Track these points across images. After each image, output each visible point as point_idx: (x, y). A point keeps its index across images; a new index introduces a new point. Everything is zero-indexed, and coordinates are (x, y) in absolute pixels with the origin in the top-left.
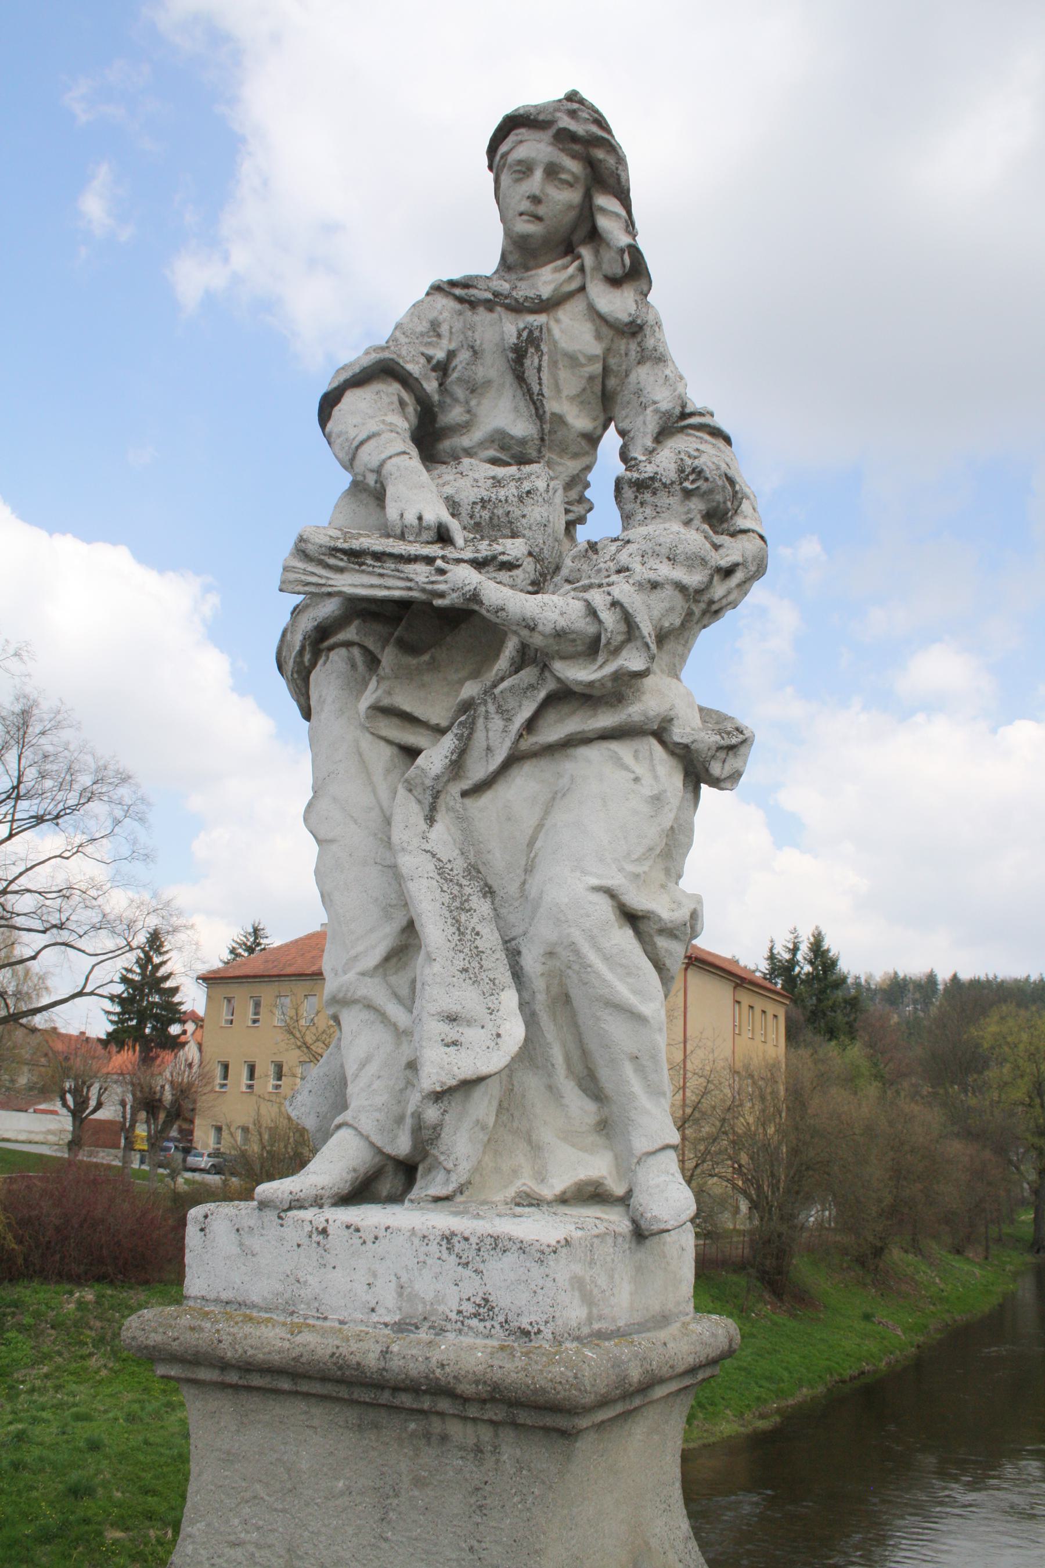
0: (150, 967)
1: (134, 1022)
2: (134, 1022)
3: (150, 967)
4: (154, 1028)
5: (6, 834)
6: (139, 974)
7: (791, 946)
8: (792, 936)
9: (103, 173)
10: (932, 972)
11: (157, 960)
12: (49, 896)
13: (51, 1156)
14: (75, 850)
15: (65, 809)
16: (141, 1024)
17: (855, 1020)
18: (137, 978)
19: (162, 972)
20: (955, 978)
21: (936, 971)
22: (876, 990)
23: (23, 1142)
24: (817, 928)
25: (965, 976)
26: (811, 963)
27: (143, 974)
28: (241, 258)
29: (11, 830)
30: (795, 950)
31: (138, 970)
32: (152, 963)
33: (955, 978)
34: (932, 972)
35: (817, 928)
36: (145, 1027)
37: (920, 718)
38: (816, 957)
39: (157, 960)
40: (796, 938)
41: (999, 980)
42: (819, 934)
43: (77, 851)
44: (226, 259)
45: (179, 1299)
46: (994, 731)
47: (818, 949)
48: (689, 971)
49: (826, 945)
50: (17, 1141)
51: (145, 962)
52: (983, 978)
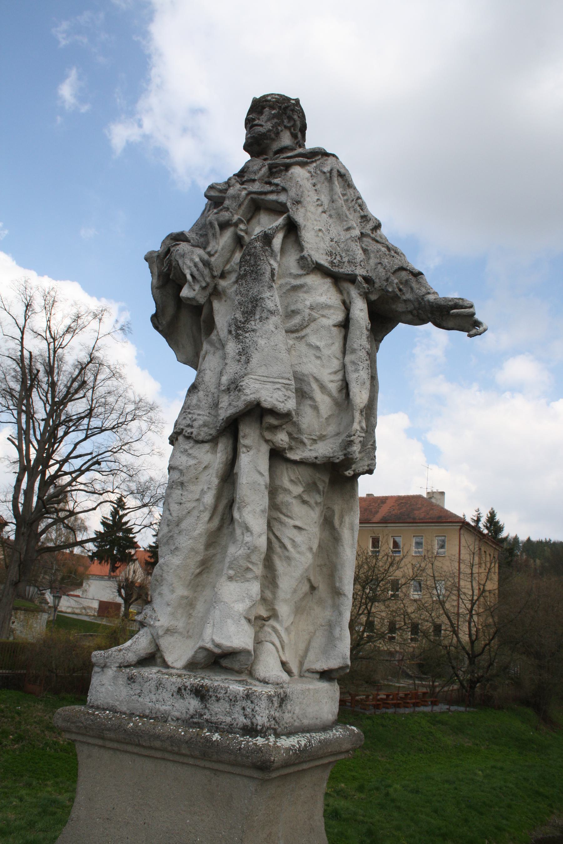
0: (117, 517)
1: (108, 547)
2: (108, 547)
3: (117, 517)
4: (118, 551)
5: (83, 436)
6: (111, 520)
7: (476, 519)
8: (476, 513)
9: (73, 73)
10: (516, 536)
11: (121, 513)
12: (104, 473)
13: (89, 622)
14: (119, 447)
15: (118, 424)
16: (112, 549)
17: (511, 561)
18: (111, 523)
19: (124, 520)
20: (529, 539)
21: (519, 536)
22: (74, 554)
23: (69, 613)
24: (492, 509)
25: (534, 539)
26: (487, 528)
27: (113, 521)
28: (148, 124)
29: (87, 435)
30: (478, 521)
31: (111, 518)
32: (119, 514)
33: (529, 539)
34: (516, 536)
35: (492, 509)
36: (114, 550)
37: (507, 395)
38: (491, 526)
39: (121, 513)
40: (479, 514)
41: (552, 542)
42: (493, 512)
43: (121, 449)
44: (140, 126)
45: (83, 702)
46: (548, 404)
47: (492, 519)
48: (462, 532)
49: (498, 518)
50: (66, 613)
51: (115, 513)
52: (544, 540)
